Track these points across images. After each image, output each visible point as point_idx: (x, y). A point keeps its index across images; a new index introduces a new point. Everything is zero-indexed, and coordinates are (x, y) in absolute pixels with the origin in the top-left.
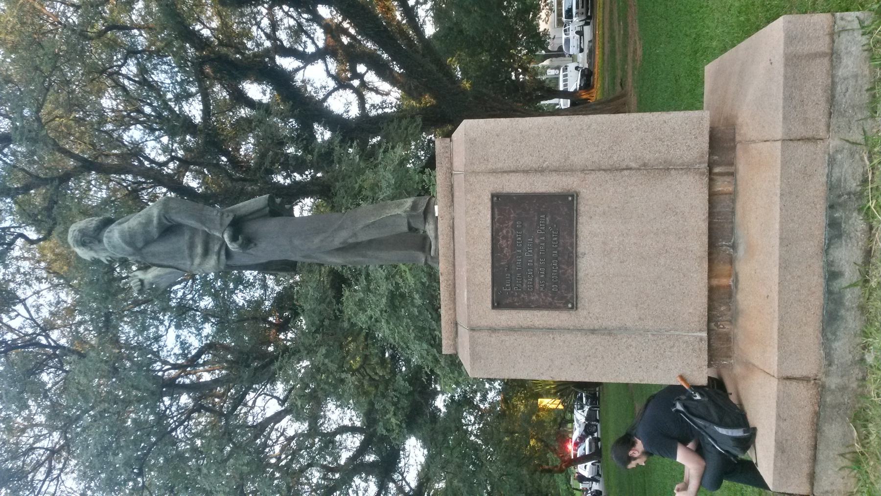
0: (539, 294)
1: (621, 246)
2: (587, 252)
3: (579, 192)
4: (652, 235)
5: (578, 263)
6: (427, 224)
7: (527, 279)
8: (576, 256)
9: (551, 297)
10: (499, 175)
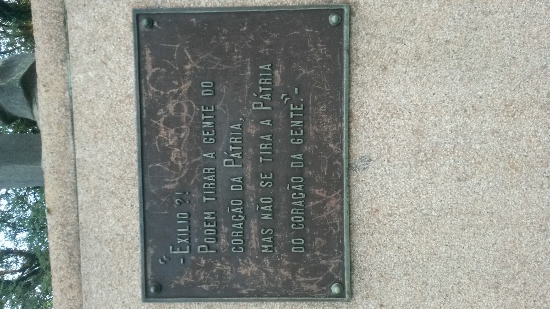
0: (258, 262)
1: (461, 140)
2: (374, 156)
3: (356, 4)
4: (536, 111)
5: (353, 182)
6: (35, 106)
7: (229, 223)
8: (350, 165)
9: (287, 268)
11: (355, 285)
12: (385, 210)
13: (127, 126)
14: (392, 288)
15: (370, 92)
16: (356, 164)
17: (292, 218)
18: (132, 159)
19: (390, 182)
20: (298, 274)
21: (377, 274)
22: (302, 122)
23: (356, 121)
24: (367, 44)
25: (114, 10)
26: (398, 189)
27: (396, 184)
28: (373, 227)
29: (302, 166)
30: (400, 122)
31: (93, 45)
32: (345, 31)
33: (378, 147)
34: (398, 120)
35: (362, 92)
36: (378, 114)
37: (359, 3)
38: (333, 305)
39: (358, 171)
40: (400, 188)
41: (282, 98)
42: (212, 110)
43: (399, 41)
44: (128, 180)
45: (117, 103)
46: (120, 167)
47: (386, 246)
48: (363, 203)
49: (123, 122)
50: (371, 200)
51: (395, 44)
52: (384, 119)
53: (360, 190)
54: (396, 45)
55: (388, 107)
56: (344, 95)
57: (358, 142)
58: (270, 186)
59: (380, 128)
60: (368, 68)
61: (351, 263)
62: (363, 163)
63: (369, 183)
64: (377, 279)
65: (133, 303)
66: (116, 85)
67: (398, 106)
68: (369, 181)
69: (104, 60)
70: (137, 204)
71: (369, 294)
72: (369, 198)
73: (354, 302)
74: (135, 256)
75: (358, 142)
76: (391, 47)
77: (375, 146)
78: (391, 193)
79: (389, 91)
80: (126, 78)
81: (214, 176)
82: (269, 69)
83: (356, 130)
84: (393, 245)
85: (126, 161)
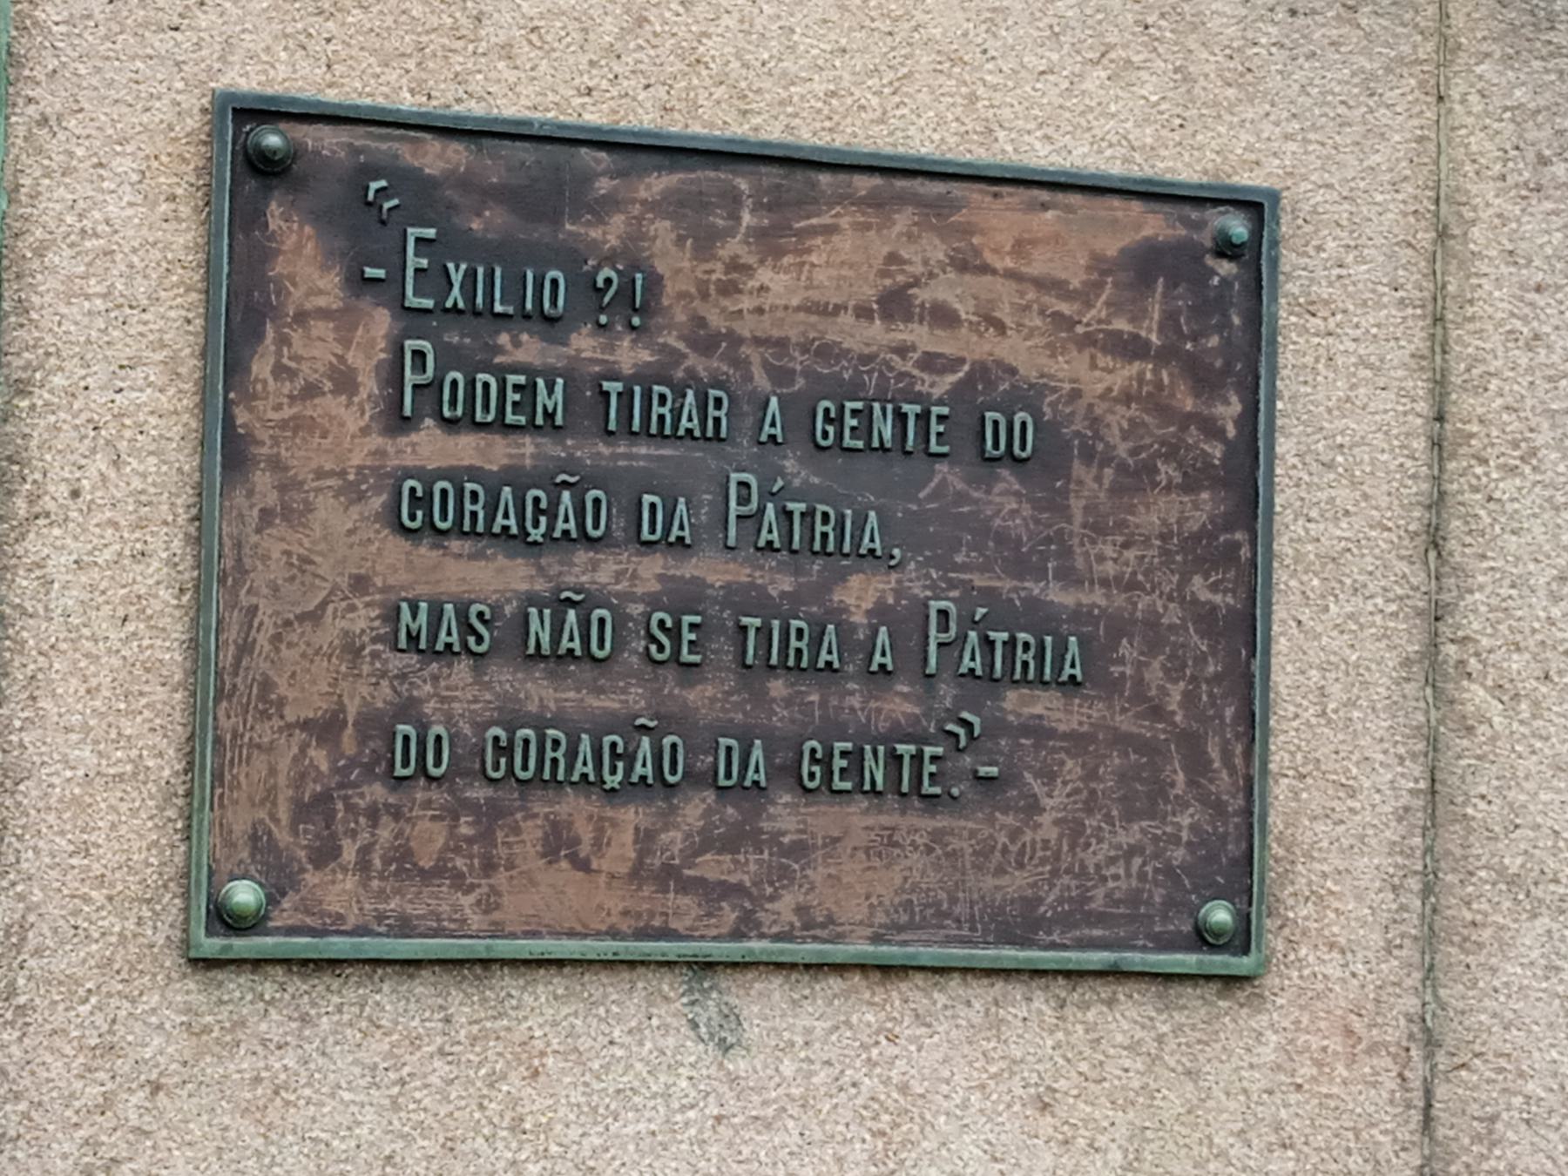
2: (738, 1064)
3: (1258, 1002)
5: (644, 982)
8: (708, 966)
10: (1413, 281)
11: (241, 980)
12: (534, 1102)
13: (884, 113)
14: (226, 1129)
15: (966, 1049)
16: (714, 995)
17: (528, 732)
18: (766, 116)
19: (642, 1127)
20: (303, 748)
21: (286, 1068)
22: (880, 786)
23: (867, 995)
24: (1127, 1042)
25: (1272, 118)
26: (613, 1158)
27: (631, 1147)
28: (472, 1057)
29: (722, 782)
30: (857, 1164)
31: (1163, 23)
32: (1180, 956)
33: (771, 1078)
34: (865, 1156)
35: (969, 1021)
36: (886, 1082)
37: (1260, 1012)
38: (165, 886)
39: (685, 1000)
40: (618, 1163)
41: (965, 715)
42: (934, 447)
43: (1131, 1156)
44: (687, 89)
45: (965, 83)
46: (735, 64)
47: (395, 1106)
48: (566, 1018)
49: (897, 99)
50: (576, 1049)
51: (1124, 1143)
52: (871, 1103)
53: (615, 1009)
54: (1120, 1147)
55: (912, 1119)
56: (966, 951)
57: (794, 1002)
58: (653, 648)
59: (841, 1089)
60: (1050, 1043)
61: (333, 964)
62: (717, 1020)
63: (641, 1044)
64: (267, 1068)
65: (198, 46)
66: (1028, 89)
67: (914, 1155)
68: (648, 1045)
69: (1113, 55)
70: (595, 116)
71: (205, 1038)
72: (584, 1043)
73: (173, 974)
74: (392, 76)
75: (794, 1002)
76: (1112, 1129)
77: (777, 1070)
78: (600, 1129)
79: (965, 1121)
80: (1050, 131)
81: (697, 433)
82: (1068, 671)
83: (835, 996)
84: (403, 1136)
85: (759, 91)
